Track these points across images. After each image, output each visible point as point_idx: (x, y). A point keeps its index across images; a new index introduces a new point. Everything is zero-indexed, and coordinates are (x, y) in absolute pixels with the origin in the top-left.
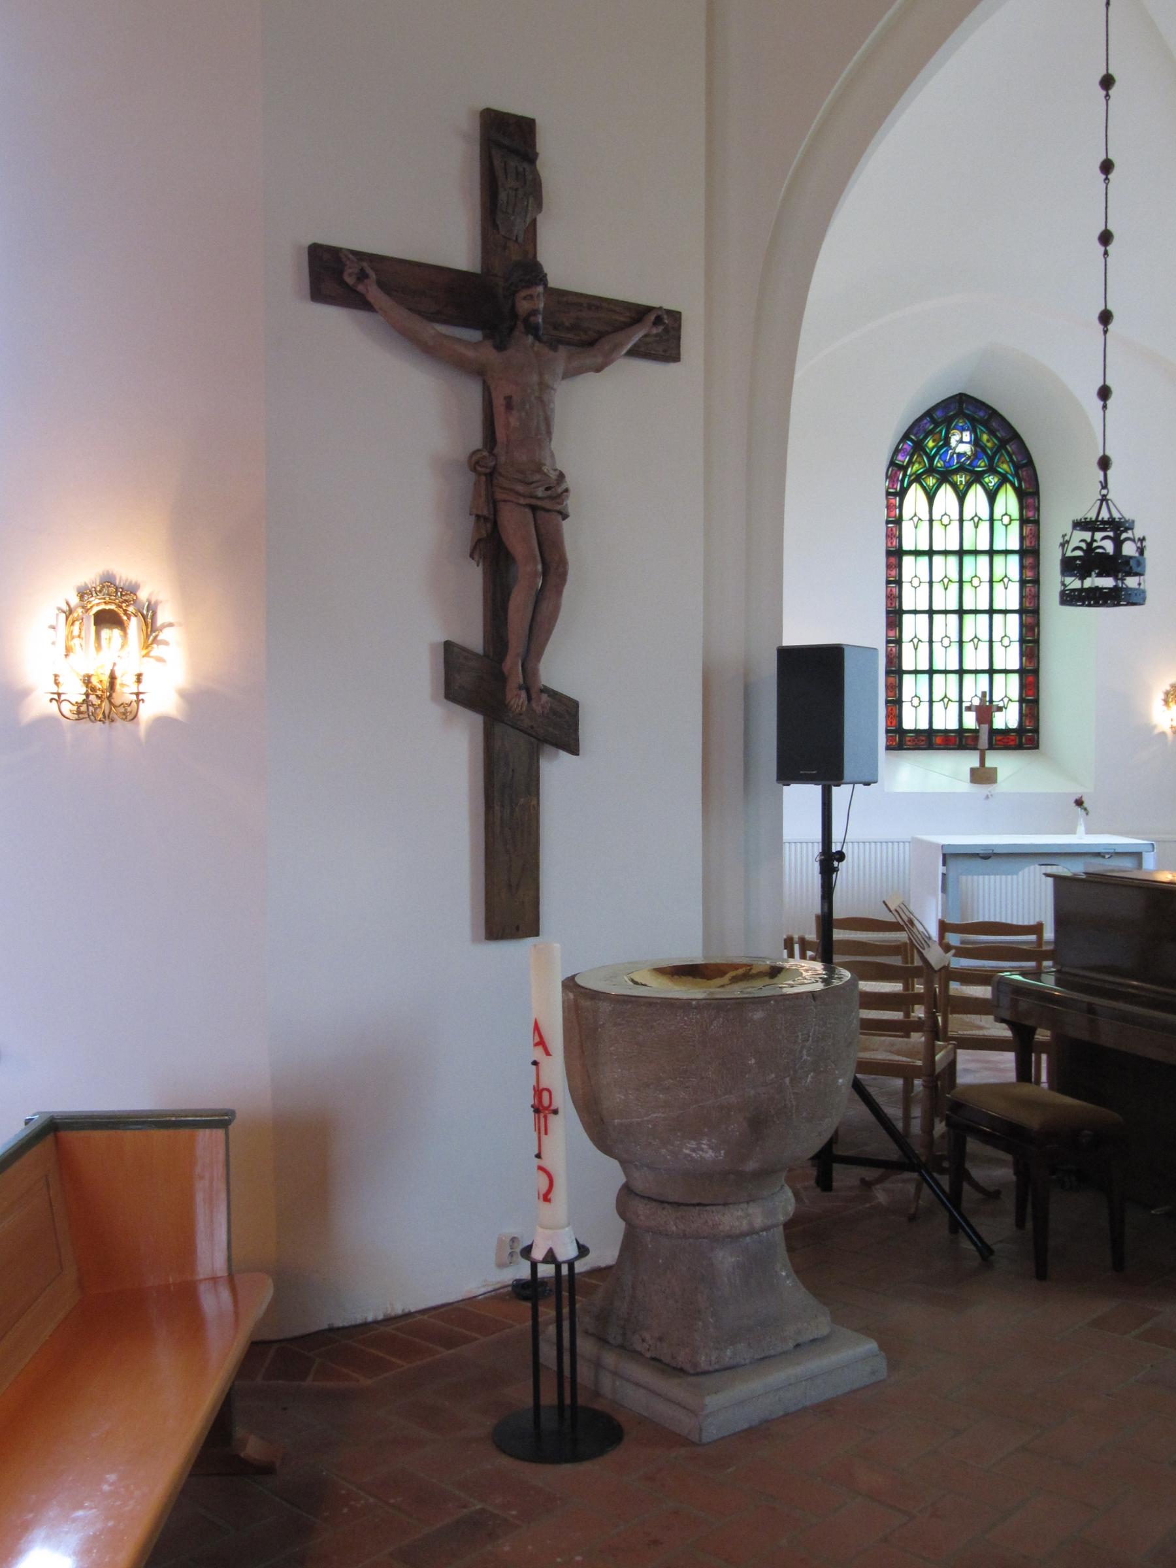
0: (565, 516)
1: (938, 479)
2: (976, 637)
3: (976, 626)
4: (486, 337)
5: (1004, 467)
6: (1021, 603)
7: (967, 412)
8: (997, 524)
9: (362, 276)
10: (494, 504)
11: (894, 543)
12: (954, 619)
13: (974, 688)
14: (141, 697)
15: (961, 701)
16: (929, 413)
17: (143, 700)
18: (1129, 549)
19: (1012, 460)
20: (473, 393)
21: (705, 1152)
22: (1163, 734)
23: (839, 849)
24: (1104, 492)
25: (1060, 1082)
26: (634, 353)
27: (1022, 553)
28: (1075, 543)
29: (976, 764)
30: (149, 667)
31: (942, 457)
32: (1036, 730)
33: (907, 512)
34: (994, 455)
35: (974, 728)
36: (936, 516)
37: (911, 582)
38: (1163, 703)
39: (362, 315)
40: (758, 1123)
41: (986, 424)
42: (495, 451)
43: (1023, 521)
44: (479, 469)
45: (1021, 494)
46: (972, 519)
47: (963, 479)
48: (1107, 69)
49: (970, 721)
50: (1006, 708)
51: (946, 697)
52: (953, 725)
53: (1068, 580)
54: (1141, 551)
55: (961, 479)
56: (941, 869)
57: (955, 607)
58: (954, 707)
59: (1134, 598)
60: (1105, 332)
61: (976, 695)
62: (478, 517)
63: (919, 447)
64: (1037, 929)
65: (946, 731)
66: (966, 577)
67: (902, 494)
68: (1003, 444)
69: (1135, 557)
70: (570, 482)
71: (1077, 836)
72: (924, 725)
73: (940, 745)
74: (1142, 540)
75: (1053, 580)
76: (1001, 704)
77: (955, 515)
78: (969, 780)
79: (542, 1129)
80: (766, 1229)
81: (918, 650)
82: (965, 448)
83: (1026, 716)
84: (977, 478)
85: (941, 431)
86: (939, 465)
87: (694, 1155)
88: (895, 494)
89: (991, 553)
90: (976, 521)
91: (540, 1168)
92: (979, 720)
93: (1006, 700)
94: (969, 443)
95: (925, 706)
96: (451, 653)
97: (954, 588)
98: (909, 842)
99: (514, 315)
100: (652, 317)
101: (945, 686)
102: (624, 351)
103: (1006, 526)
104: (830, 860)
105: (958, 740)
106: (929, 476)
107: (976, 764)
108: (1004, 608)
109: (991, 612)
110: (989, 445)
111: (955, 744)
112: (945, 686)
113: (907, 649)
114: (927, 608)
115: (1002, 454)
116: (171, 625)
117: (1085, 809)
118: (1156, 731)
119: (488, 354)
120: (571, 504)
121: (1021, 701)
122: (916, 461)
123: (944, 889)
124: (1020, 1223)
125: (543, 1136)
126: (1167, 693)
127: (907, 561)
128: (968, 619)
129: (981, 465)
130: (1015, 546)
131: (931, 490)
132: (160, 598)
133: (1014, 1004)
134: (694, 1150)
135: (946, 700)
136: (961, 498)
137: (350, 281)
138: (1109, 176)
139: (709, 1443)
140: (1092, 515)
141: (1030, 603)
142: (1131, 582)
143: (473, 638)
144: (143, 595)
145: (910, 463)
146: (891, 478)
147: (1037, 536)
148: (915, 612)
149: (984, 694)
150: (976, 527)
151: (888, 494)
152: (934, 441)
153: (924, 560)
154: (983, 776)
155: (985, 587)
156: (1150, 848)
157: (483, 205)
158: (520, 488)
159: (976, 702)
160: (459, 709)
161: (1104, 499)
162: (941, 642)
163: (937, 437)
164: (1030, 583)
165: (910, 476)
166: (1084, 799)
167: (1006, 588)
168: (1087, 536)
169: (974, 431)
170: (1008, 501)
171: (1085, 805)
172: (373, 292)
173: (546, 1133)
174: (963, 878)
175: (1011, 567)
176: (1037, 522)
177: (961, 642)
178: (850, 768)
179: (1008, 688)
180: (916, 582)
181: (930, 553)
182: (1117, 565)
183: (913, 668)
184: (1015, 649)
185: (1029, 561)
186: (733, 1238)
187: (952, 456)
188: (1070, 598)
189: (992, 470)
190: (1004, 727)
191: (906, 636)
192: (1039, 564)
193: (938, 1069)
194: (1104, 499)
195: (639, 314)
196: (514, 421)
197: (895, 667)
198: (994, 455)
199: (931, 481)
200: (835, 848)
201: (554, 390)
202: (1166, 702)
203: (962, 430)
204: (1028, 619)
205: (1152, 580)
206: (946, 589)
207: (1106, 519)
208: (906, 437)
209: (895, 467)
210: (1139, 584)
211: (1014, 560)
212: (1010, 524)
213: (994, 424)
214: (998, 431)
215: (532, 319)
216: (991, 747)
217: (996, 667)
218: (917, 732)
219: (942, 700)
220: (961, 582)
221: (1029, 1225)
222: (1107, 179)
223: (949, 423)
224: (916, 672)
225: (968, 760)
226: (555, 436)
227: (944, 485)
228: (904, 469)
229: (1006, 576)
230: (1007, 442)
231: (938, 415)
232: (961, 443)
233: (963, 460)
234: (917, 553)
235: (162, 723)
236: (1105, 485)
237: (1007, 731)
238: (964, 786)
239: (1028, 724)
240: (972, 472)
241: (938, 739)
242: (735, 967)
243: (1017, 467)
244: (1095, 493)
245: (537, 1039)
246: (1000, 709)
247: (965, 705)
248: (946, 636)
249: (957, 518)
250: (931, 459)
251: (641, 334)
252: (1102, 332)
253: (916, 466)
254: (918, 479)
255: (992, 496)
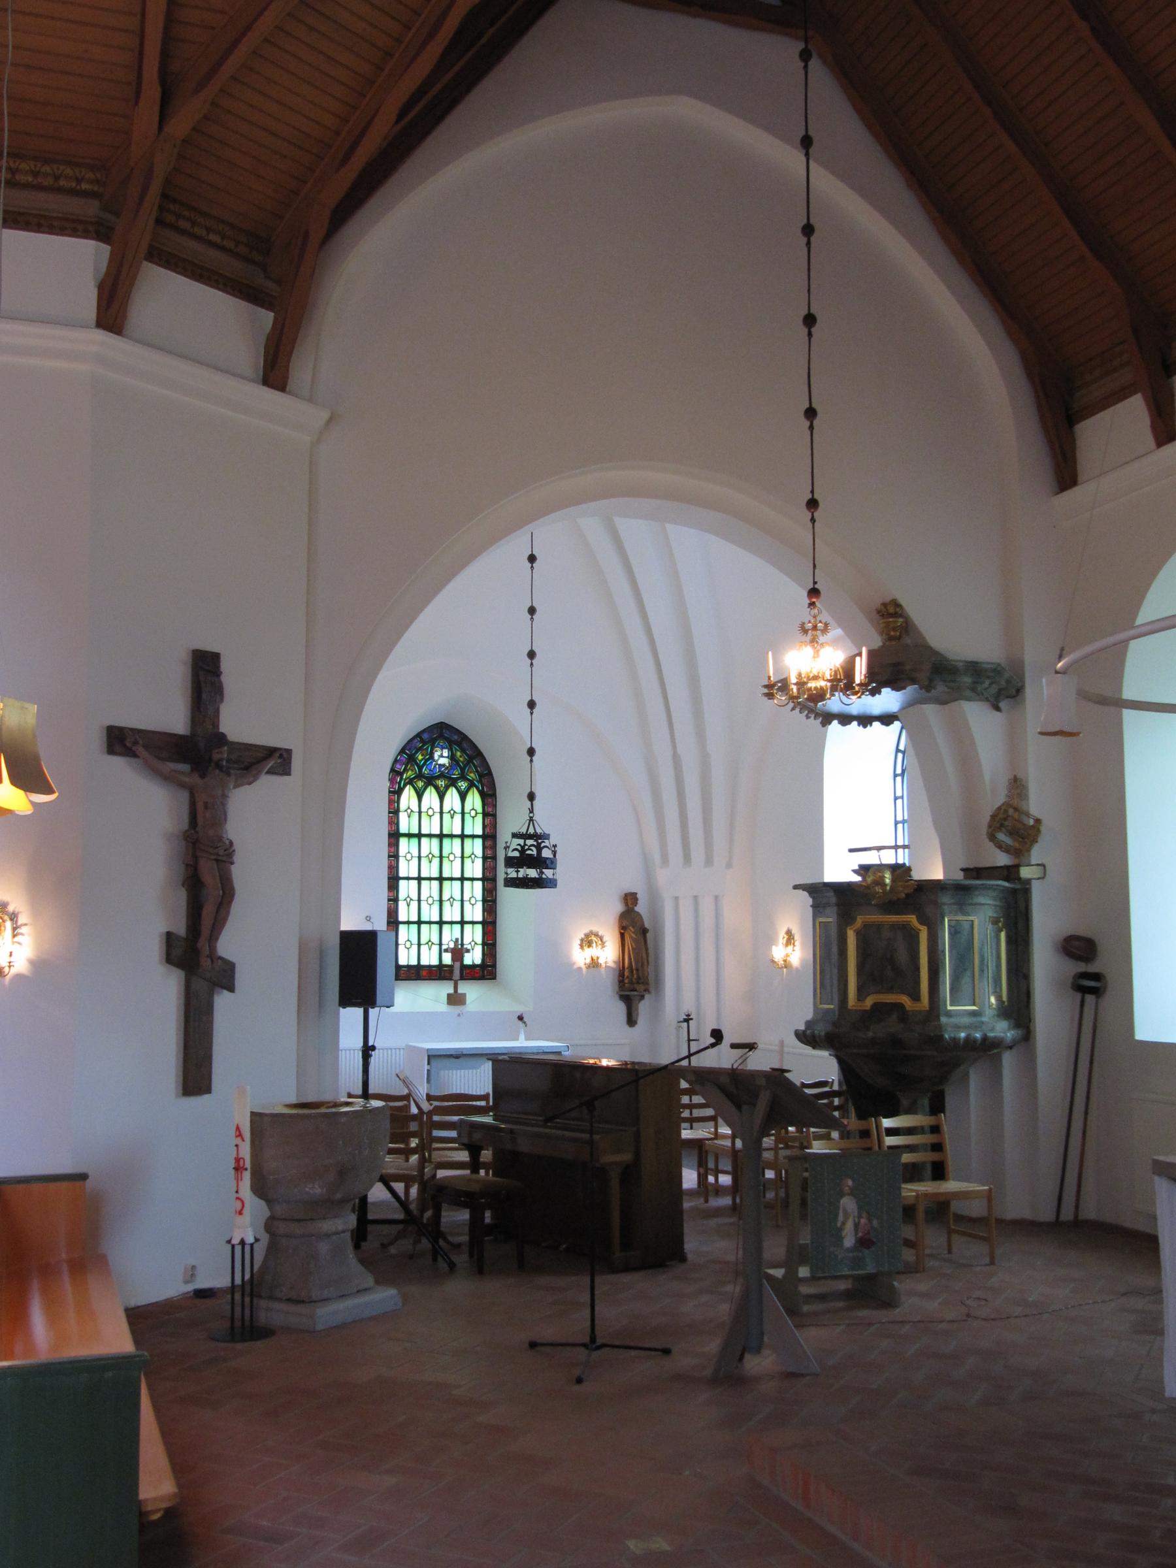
0: (232, 863)
1: (425, 783)
2: (452, 897)
3: (452, 889)
4: (192, 770)
5: (472, 776)
6: (483, 873)
7: (446, 735)
8: (467, 817)
9: (136, 743)
10: (196, 858)
11: (393, 828)
12: (435, 884)
13: (450, 935)
14: (11, 964)
15: (440, 944)
16: (419, 735)
17: (13, 966)
18: (546, 853)
19: (477, 771)
20: (184, 796)
21: (316, 1190)
22: (580, 969)
23: (372, 1044)
24: (531, 815)
25: (494, 1175)
26: (269, 772)
27: (484, 837)
28: (513, 846)
29: (452, 991)
30: (15, 949)
31: (428, 767)
32: (494, 966)
33: (403, 805)
34: (465, 766)
35: (450, 964)
36: (424, 809)
37: (405, 857)
38: (579, 947)
39: (133, 760)
40: (343, 1173)
41: (459, 744)
42: (197, 829)
43: (485, 814)
44: (188, 839)
45: (483, 795)
46: (449, 812)
47: (443, 783)
48: (532, 551)
49: (447, 959)
50: (473, 949)
51: (430, 941)
52: (435, 962)
53: (509, 870)
54: (555, 853)
55: (441, 783)
56: (426, 1067)
57: (437, 919)
58: (436, 949)
59: (550, 884)
60: (532, 714)
61: (452, 940)
62: (187, 865)
63: (411, 759)
64: (485, 1097)
65: (430, 966)
66: (445, 854)
67: (399, 792)
68: (470, 760)
69: (550, 858)
70: (236, 846)
71: (519, 1041)
72: (414, 962)
73: (425, 976)
74: (555, 846)
75: (502, 872)
76: (469, 947)
77: (437, 809)
78: (446, 1002)
79: (238, 1179)
80: (343, 1232)
81: (410, 907)
82: (444, 761)
83: (487, 955)
84: (453, 783)
85: (428, 748)
86: (426, 772)
87: (311, 1191)
88: (394, 792)
89: (463, 837)
90: (452, 814)
91: (238, 1198)
92: (453, 959)
93: (473, 943)
94: (447, 757)
95: (415, 948)
96: (170, 938)
97: (436, 861)
98: (403, 1049)
99: (210, 760)
100: (277, 754)
101: (429, 933)
102: (265, 771)
103: (473, 817)
104: (367, 1051)
105: (438, 973)
106: (419, 780)
107: (452, 991)
108: (472, 877)
109: (462, 879)
110: (461, 759)
111: (436, 976)
112: (429, 933)
113: (402, 906)
114: (416, 875)
115: (470, 766)
116: (25, 925)
117: (525, 1023)
118: (575, 967)
119: (195, 779)
120: (236, 858)
121: (484, 944)
122: (409, 769)
123: (428, 1081)
124: (471, 1255)
125: (239, 1181)
126: (582, 940)
127: (403, 842)
128: (446, 884)
129: (456, 774)
130: (480, 832)
131: (420, 790)
132: (20, 910)
133: (470, 1134)
134: (310, 1189)
135: (430, 943)
136: (442, 797)
137: (128, 745)
138: (534, 617)
139: (318, 1331)
140: (524, 830)
141: (490, 873)
142: (548, 873)
143: (181, 929)
144: (11, 908)
145: (406, 770)
146: (392, 781)
147: (494, 825)
148: (408, 878)
149: (457, 940)
150: (452, 818)
151: (390, 792)
152: (422, 755)
153: (415, 841)
154: (455, 999)
155: (459, 861)
156: (566, 1049)
157: (193, 698)
158: (211, 850)
159: (452, 945)
160: (174, 969)
161: (531, 820)
162: (427, 900)
163: (424, 752)
164: (489, 859)
165: (406, 779)
166: (524, 1015)
167: (473, 862)
168: (521, 842)
169: (450, 749)
170: (474, 800)
171: (525, 1019)
172: (140, 750)
173: (241, 1180)
174: (442, 1073)
175: (476, 847)
176: (494, 816)
177: (441, 901)
178: (380, 998)
179: (475, 935)
180: (409, 856)
181: (419, 836)
182: (539, 862)
183: (406, 920)
184: (479, 906)
185: (488, 843)
186: (328, 1235)
187: (435, 767)
188: (511, 883)
189: (463, 777)
190: (471, 964)
191: (402, 895)
192: (496, 844)
193: (426, 1178)
194: (531, 820)
195: (271, 752)
196: (208, 815)
197: (393, 918)
198: (465, 766)
199: (420, 784)
200: (370, 1044)
201: (228, 797)
202: (582, 947)
203: (442, 748)
204: (489, 885)
205: (560, 873)
206: (430, 862)
207: (532, 833)
208: (402, 751)
209: (394, 773)
210: (554, 875)
211: (479, 842)
212: (476, 816)
213: (465, 745)
214: (468, 750)
215: (221, 762)
216: (462, 978)
217: (466, 919)
218: (409, 967)
219: (427, 943)
220: (441, 857)
221: (476, 1257)
222: (532, 618)
223: (433, 743)
224: (408, 923)
225: (447, 988)
226: (228, 823)
227: (429, 787)
228: (401, 774)
229: (473, 854)
230: (474, 758)
231: (425, 736)
232: (442, 757)
233: (443, 769)
234: (409, 836)
235: (19, 977)
236: (531, 811)
237: (474, 966)
238: (442, 1007)
239: (488, 961)
240: (450, 779)
241: (424, 972)
242: (328, 1103)
243: (481, 776)
244: (526, 816)
245: (238, 1133)
246: (468, 951)
247: (444, 947)
248: (430, 896)
249: (439, 811)
250: (420, 768)
251: (273, 762)
252: (529, 714)
253: (410, 773)
254: (411, 782)
255: (463, 796)
